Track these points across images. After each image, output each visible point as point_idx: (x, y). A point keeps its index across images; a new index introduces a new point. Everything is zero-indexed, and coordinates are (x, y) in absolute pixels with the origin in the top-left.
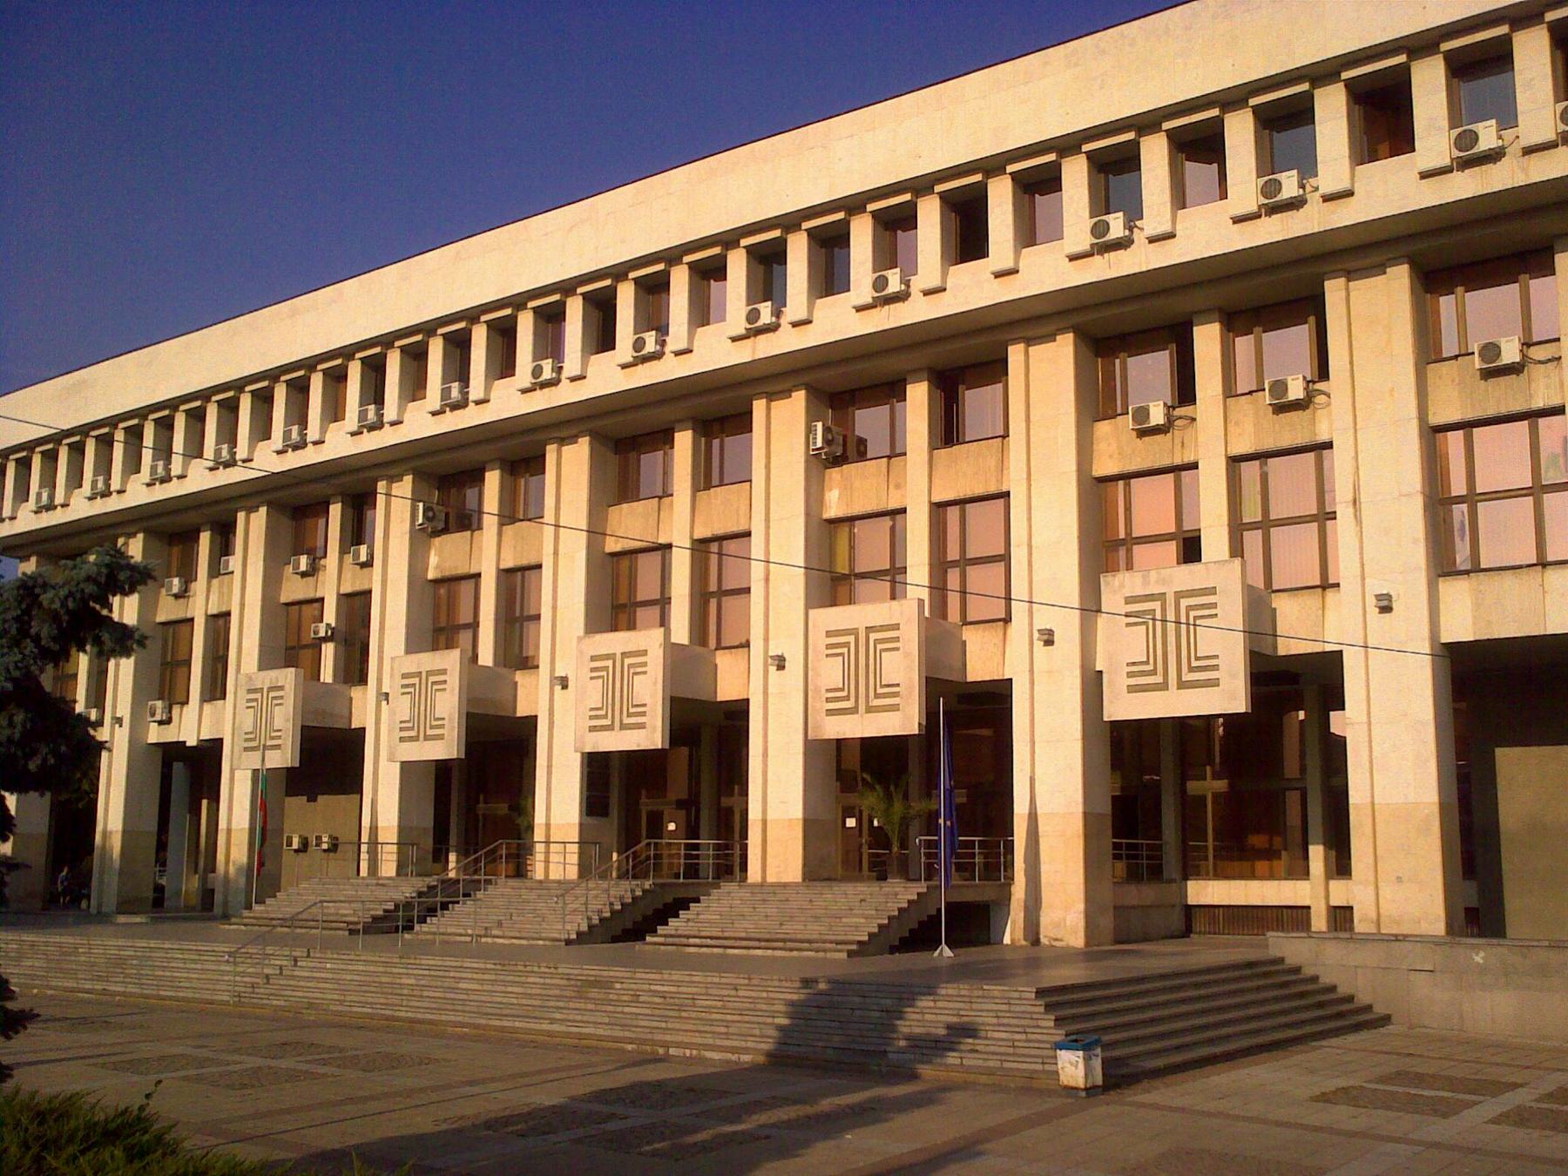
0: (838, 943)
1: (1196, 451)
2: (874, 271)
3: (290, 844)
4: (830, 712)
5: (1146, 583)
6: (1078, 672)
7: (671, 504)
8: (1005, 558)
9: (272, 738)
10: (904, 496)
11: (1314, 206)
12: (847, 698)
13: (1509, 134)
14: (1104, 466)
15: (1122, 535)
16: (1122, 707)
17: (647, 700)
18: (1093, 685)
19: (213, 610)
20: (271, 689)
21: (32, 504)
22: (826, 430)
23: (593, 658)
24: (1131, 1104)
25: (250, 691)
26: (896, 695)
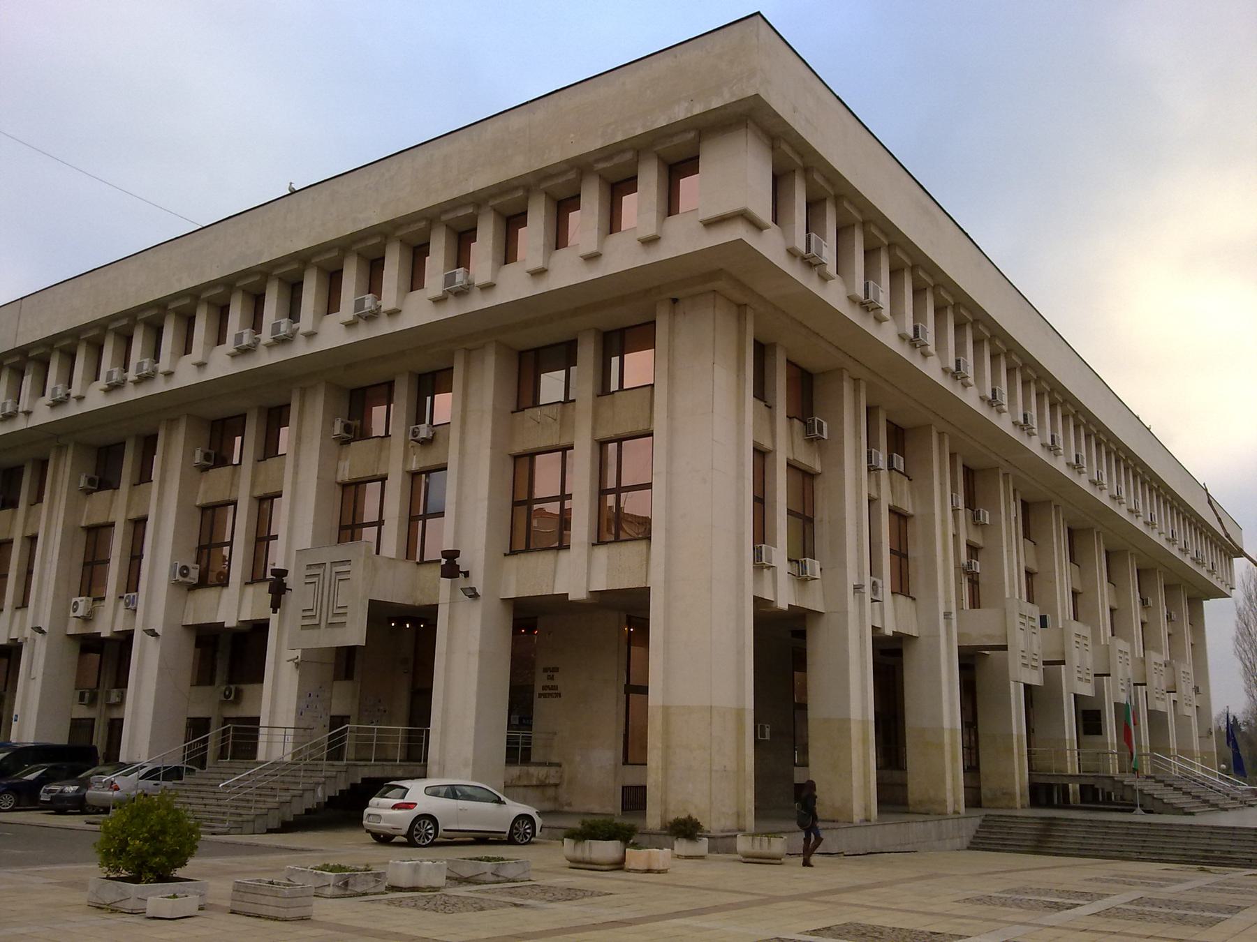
7: (574, 409)
11: (160, 379)
13: (295, 326)
19: (133, 515)
21: (230, 346)
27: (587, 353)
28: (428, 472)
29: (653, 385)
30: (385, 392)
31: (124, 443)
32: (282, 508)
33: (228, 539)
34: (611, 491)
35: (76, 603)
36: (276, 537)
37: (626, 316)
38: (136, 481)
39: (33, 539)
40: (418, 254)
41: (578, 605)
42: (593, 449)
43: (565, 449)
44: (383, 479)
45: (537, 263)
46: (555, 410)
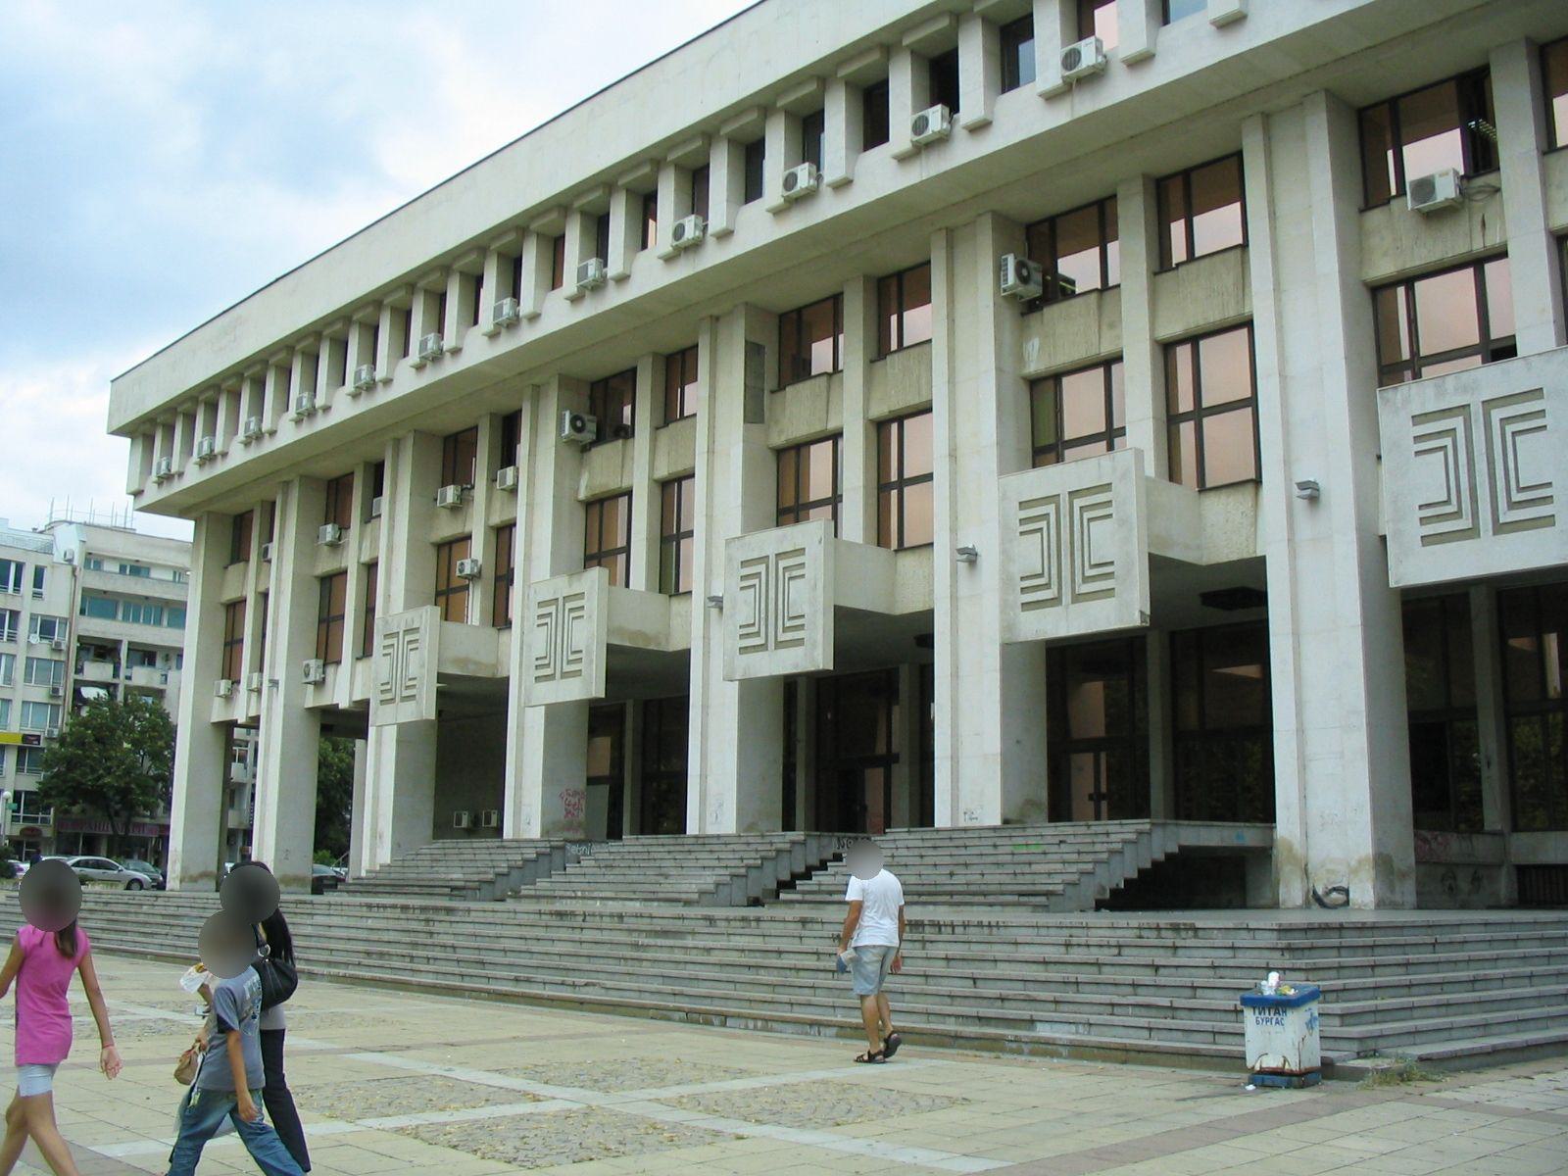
0: (1021, 894)
1: (1503, 230)
2: (1064, 44)
3: (459, 822)
4: (1026, 606)
5: (1440, 393)
6: (1353, 536)
8: (1252, 402)
9: (407, 687)
10: (1119, 337)
12: (1047, 586)
14: (1384, 267)
15: (1406, 355)
16: (1422, 565)
17: (806, 610)
18: (1376, 550)
20: (407, 632)
22: (1020, 266)
23: (744, 564)
24: (1437, 1103)
25: (386, 636)
26: (1110, 575)
28: (900, 418)
30: (826, 315)
31: (352, 473)
33: (621, 543)
34: (1186, 417)
35: (308, 665)
36: (690, 534)
37: (899, 258)
38: (874, 355)
39: (265, 595)
40: (646, 205)
41: (344, 712)
42: (867, 437)
43: (1109, 363)
44: (836, 436)
46: (824, 380)
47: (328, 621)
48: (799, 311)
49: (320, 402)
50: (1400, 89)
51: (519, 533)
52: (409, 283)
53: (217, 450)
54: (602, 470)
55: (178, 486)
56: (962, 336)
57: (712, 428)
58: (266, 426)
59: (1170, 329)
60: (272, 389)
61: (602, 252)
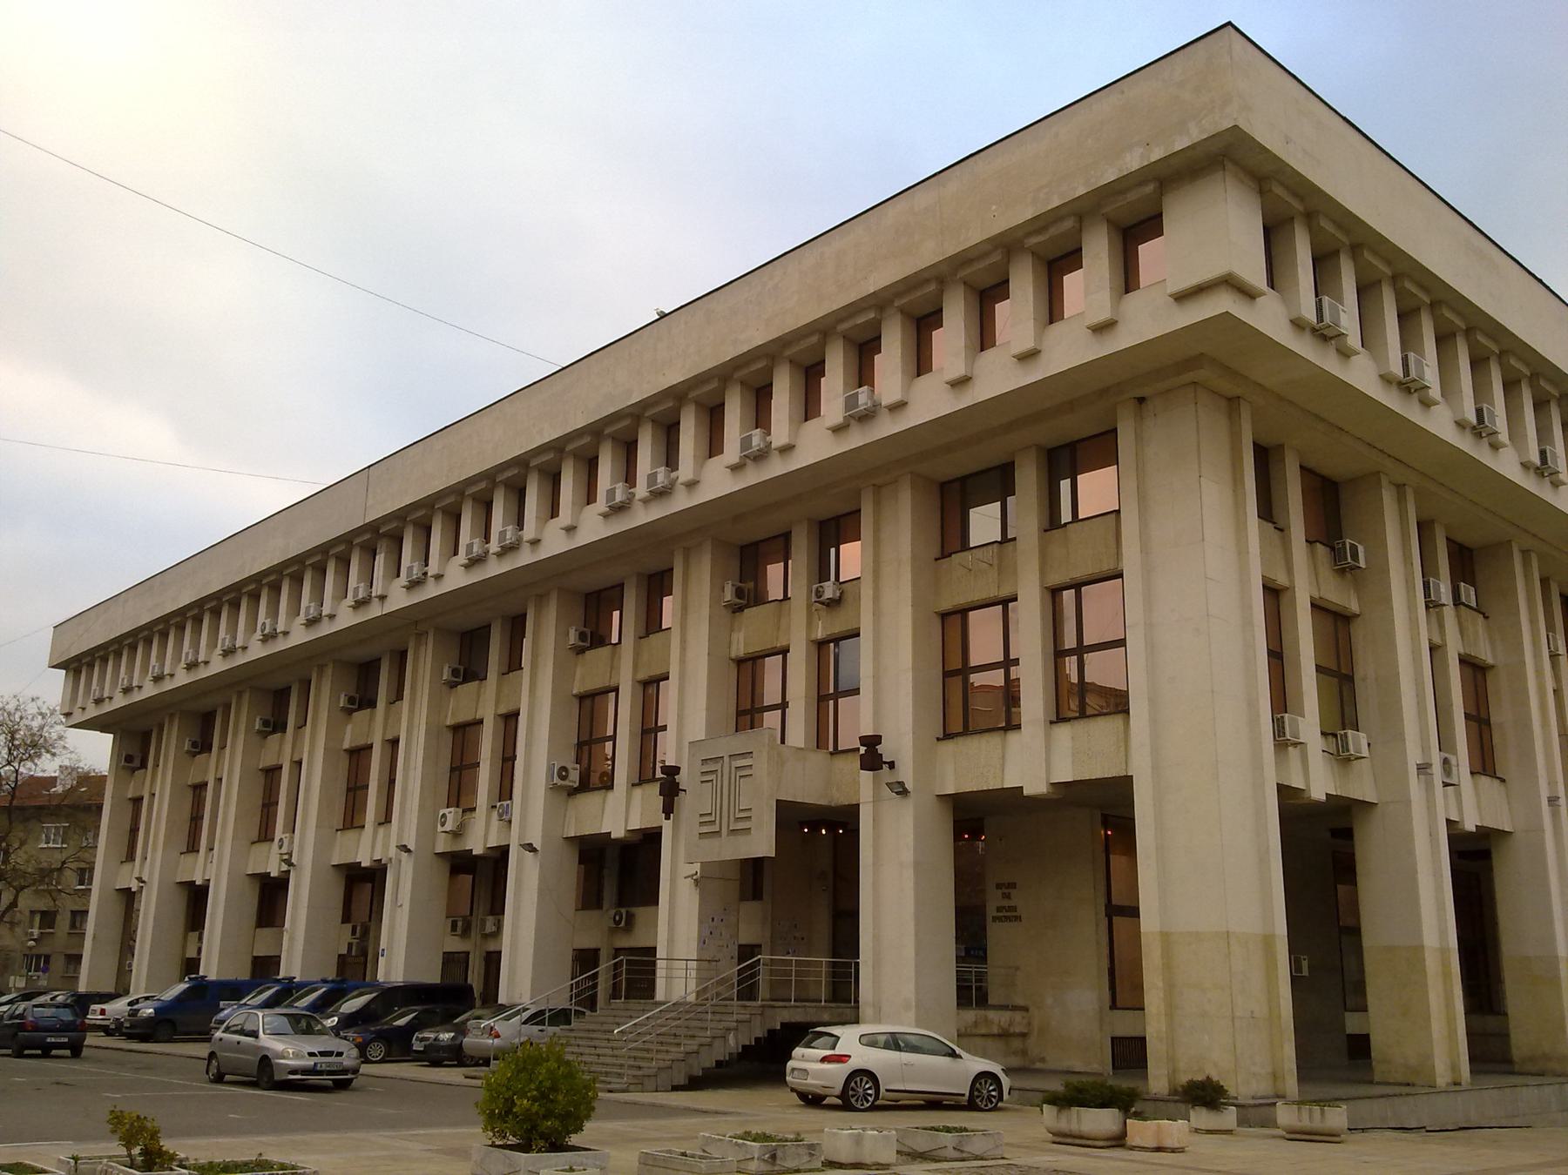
27: (1028, 478)
28: (837, 640)
29: (1118, 512)
30: (780, 545)
31: (489, 626)
32: (669, 693)
34: (1070, 652)
38: (642, 632)
39: (395, 742)
42: (1042, 599)
43: (1006, 602)
44: (784, 652)
45: (957, 369)
47: (355, 790)
48: (600, 592)
49: (135, 684)
50: (1076, 437)
51: (523, 719)
52: (458, 491)
53: (135, 684)
54: (590, 672)
55: (107, 708)
56: (882, 569)
57: (683, 641)
58: (326, 610)
59: (1056, 579)
60: (692, 431)
61: (671, 461)
